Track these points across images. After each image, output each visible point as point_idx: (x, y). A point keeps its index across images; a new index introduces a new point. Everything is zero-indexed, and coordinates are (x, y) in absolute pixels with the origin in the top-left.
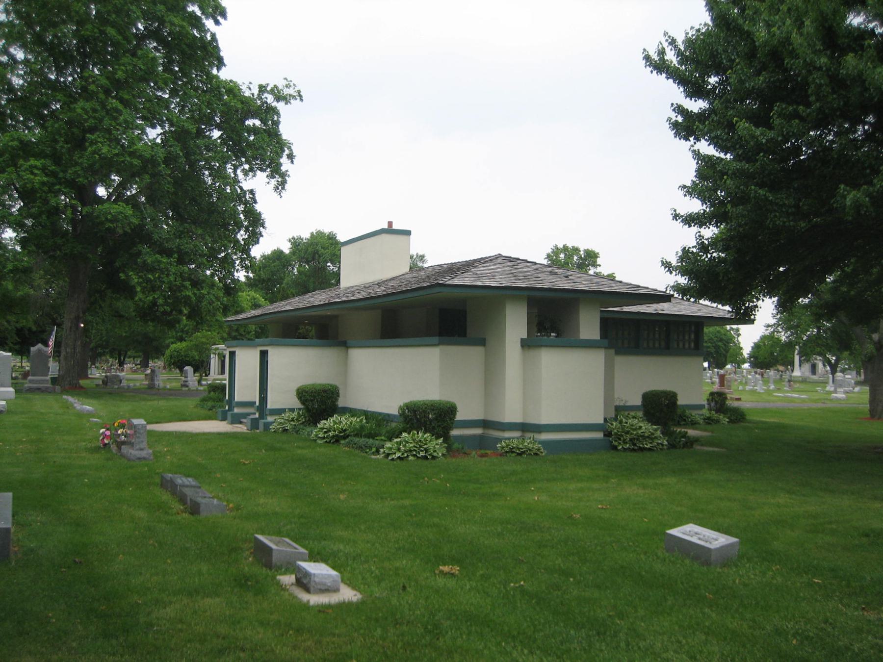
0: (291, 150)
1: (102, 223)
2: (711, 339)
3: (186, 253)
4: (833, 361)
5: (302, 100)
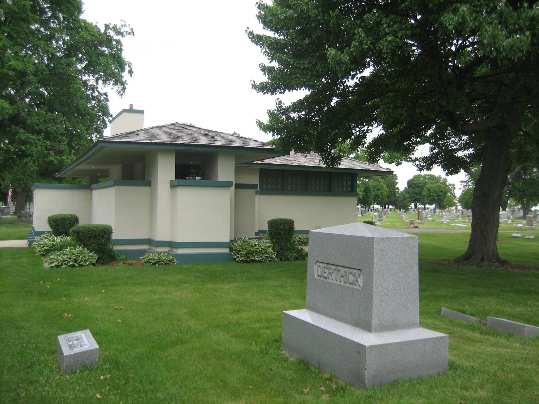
0: (131, 68)
2: (436, 191)
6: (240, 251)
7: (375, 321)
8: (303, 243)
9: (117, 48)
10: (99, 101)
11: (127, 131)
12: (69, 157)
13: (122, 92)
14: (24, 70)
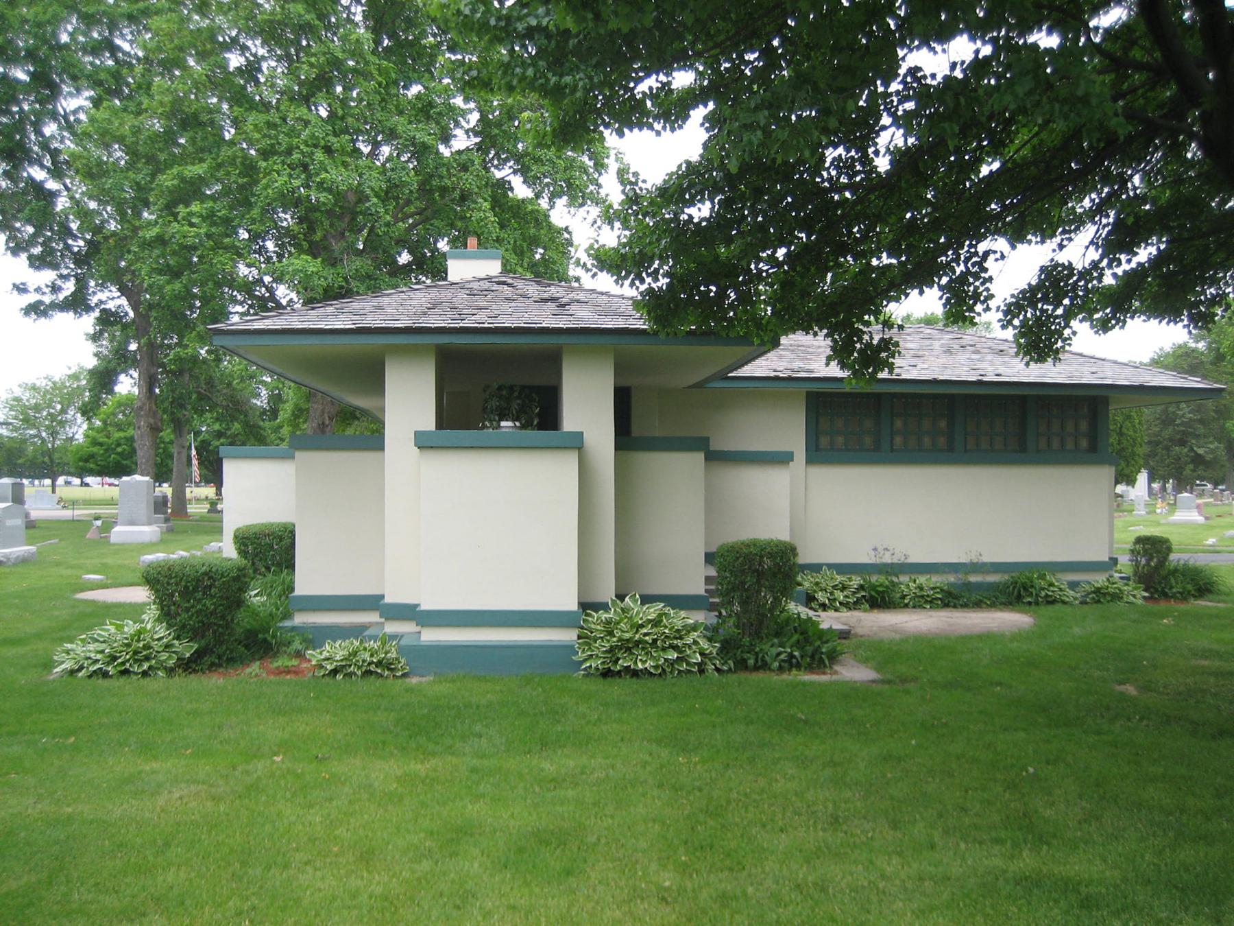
8: (926, 602)
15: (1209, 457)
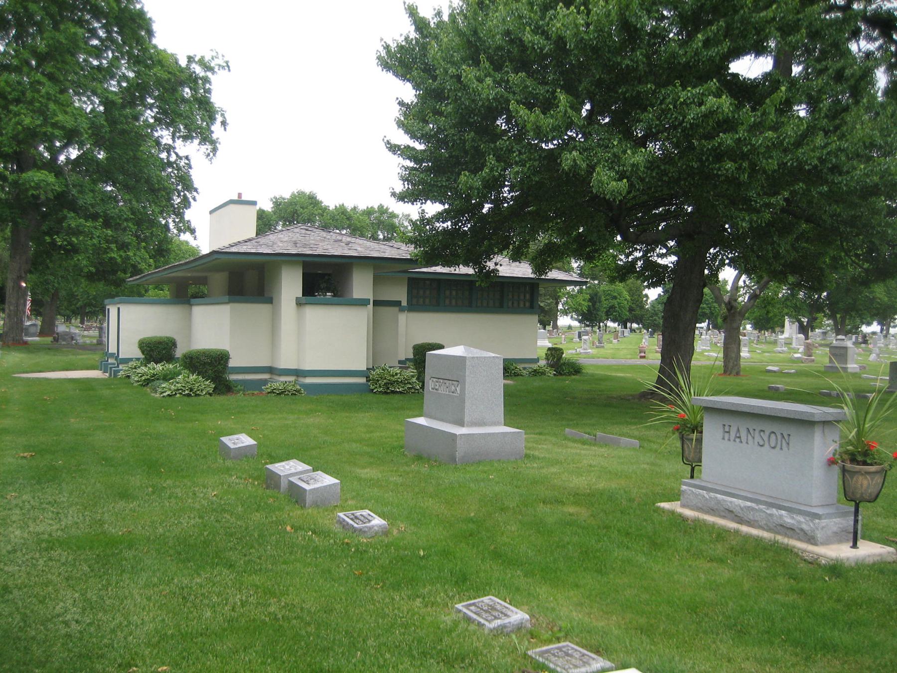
0: (224, 118)
1: (27, 190)
3: (112, 217)
4: (805, 324)
5: (229, 70)
6: (378, 380)
7: (467, 419)
9: (204, 89)
10: (179, 169)
11: (245, 238)
12: (138, 253)
13: (211, 154)
14: (76, 126)
15: (547, 308)
